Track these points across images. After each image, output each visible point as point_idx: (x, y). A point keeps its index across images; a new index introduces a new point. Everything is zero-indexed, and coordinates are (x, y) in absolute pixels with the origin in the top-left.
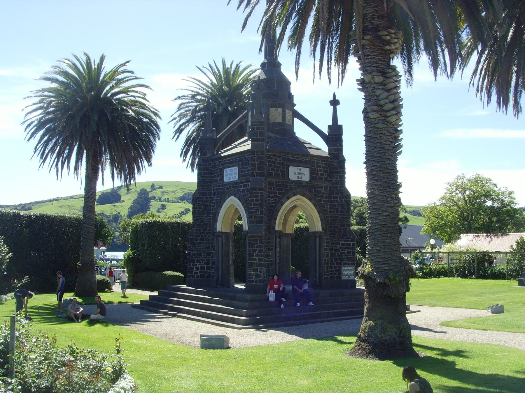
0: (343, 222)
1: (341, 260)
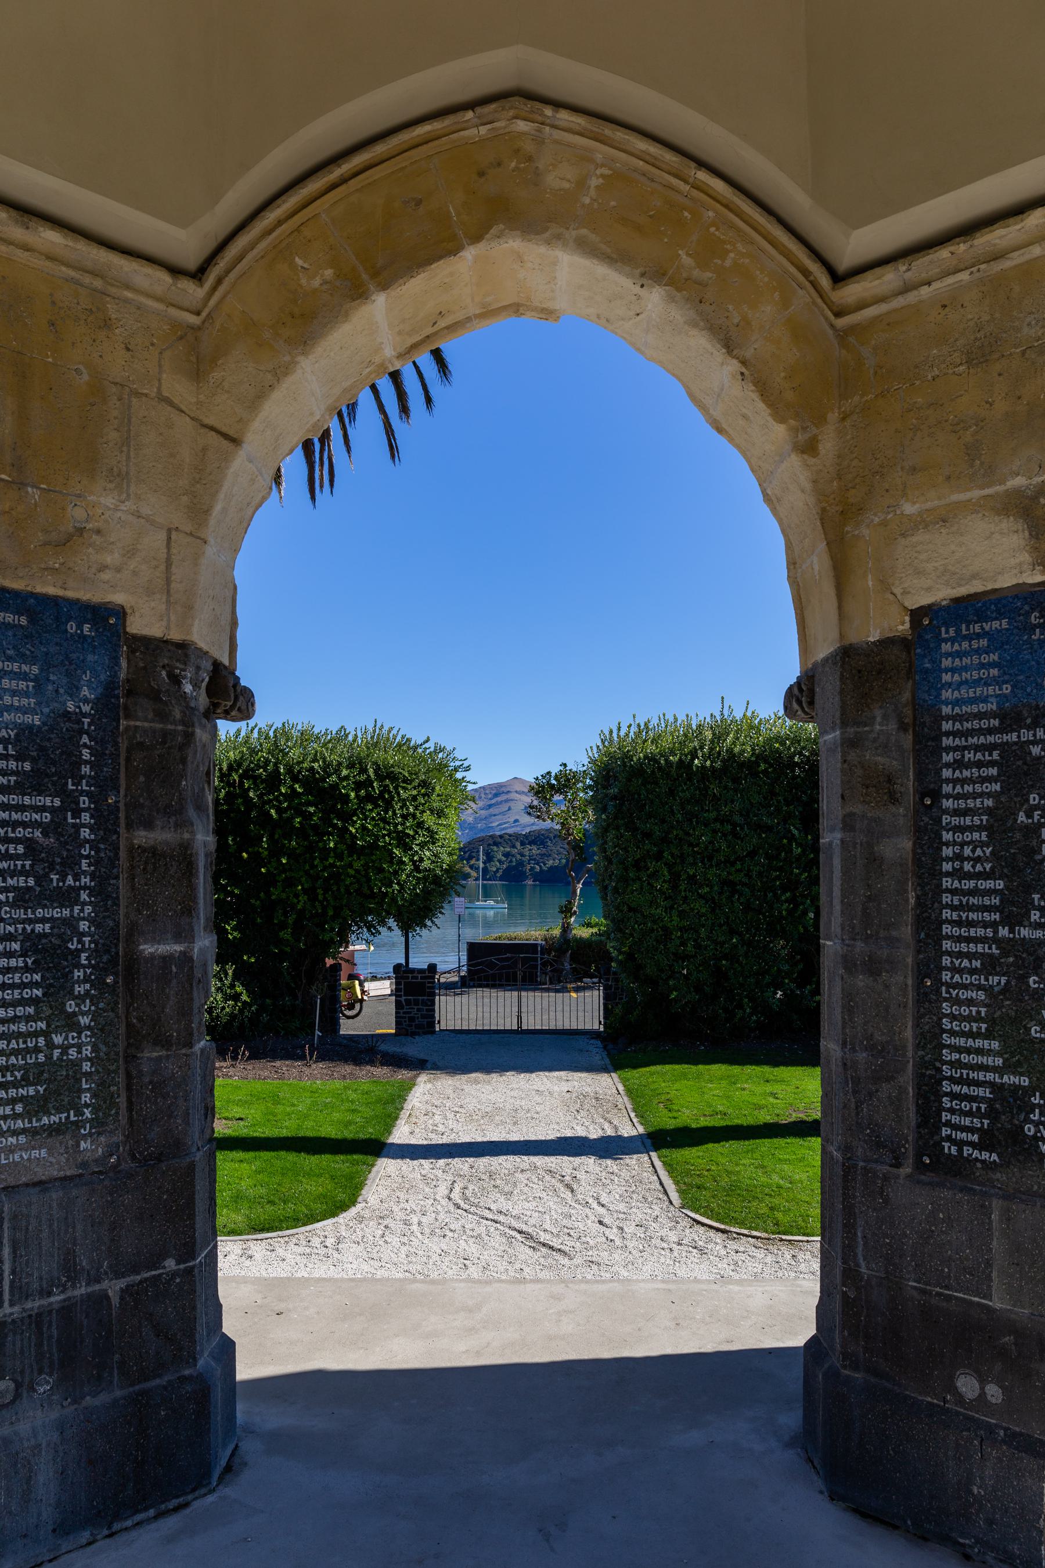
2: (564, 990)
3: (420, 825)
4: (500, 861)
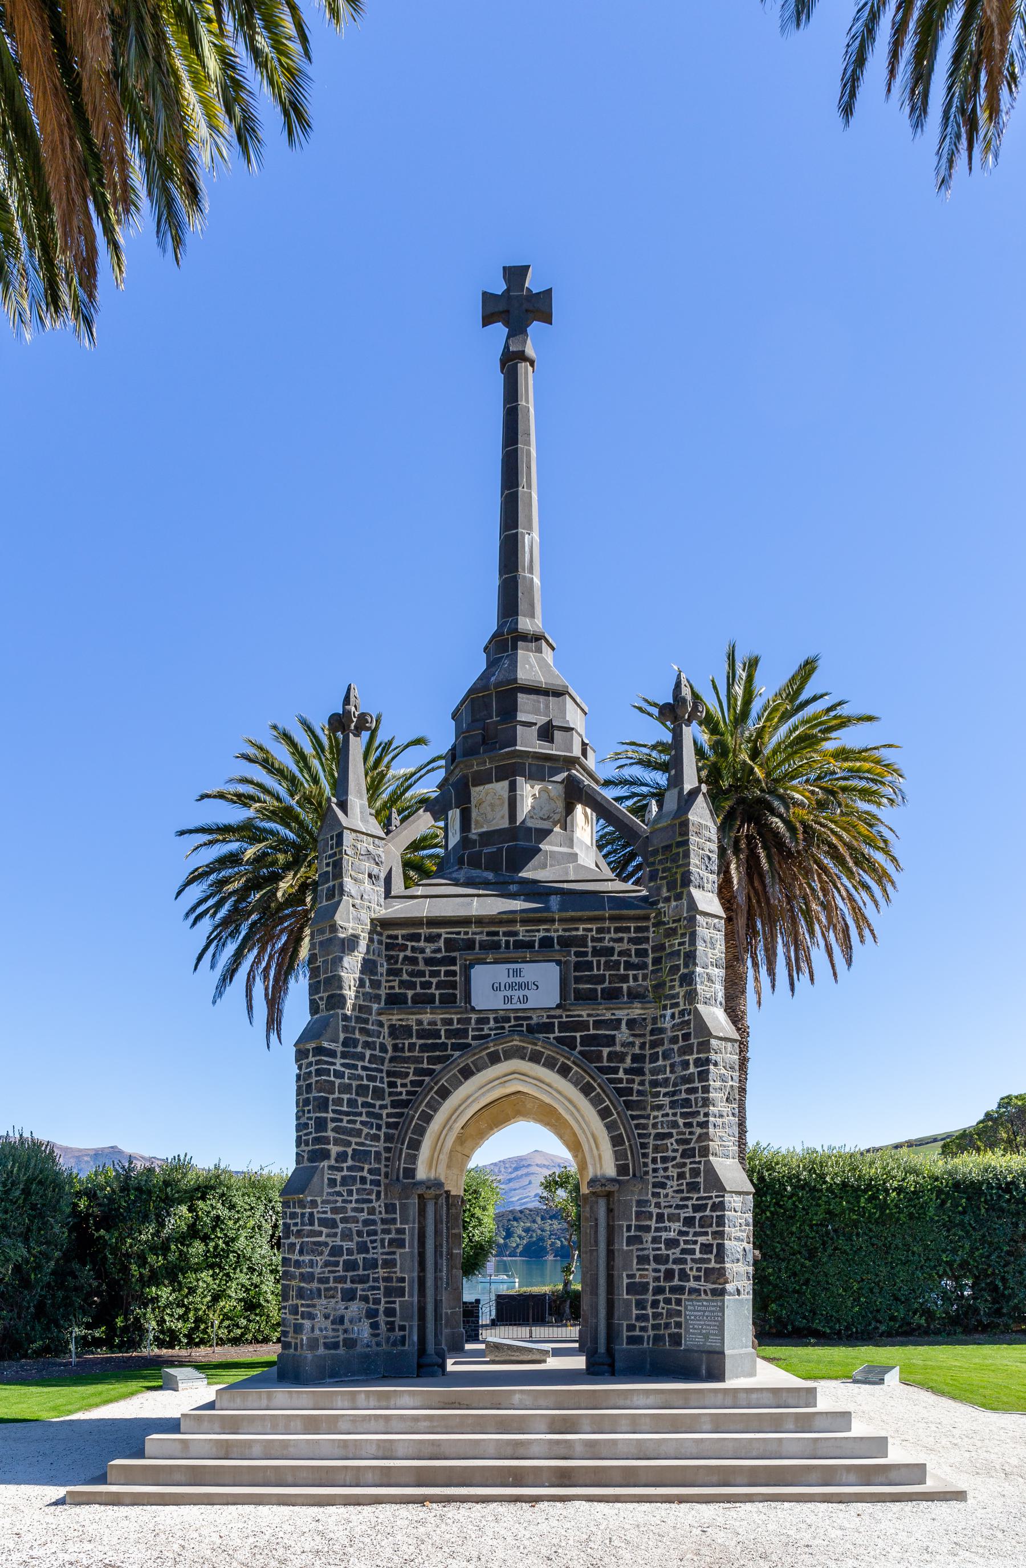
0: (687, 1142)
1: (684, 1276)
2: (566, 1326)
3: (473, 1215)
4: (520, 1237)
